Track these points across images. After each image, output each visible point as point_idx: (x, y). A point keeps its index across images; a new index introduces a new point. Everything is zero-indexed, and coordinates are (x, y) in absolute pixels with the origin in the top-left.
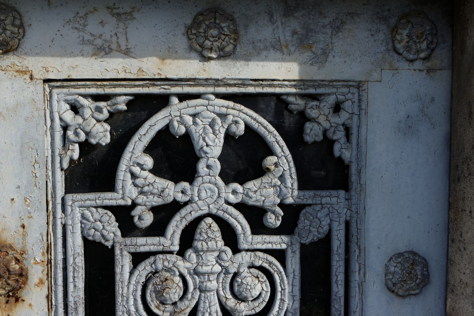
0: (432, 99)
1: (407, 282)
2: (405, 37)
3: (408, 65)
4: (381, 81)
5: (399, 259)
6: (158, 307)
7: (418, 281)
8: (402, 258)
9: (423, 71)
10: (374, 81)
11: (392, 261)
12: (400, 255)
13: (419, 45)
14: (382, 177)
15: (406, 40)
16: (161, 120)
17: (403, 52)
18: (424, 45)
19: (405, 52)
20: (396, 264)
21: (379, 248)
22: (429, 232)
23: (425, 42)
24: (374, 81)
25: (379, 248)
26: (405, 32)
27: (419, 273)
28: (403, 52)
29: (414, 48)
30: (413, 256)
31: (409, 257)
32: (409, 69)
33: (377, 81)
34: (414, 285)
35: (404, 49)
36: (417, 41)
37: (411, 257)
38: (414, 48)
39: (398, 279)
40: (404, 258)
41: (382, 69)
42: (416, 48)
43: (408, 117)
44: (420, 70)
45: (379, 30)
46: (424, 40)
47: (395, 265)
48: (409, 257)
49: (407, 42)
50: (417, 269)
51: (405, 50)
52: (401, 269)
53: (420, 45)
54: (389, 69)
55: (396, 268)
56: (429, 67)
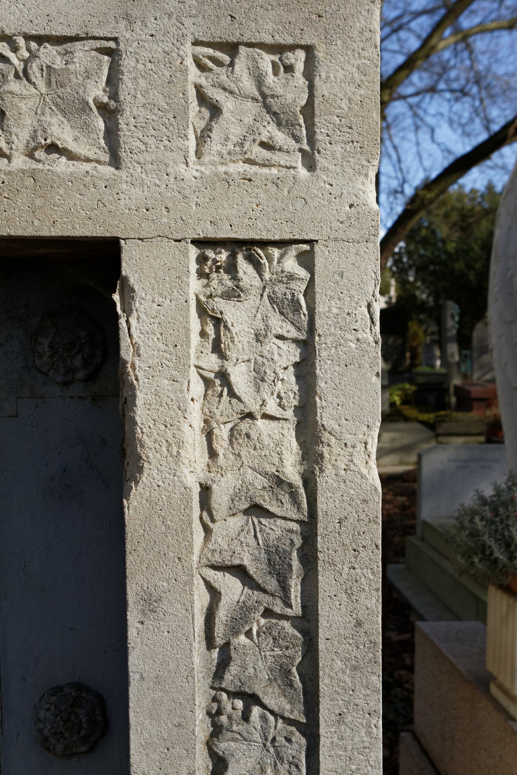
0: (103, 442)
1: (64, 734)
2: (47, 349)
3: (61, 390)
4: (17, 416)
5: (53, 697)
6: (291, 733)
7: (83, 733)
8: (59, 695)
9: (86, 398)
10: (5, 417)
11: (43, 700)
12: (57, 690)
13: (69, 360)
14: (25, 566)
15: (48, 354)
16: (132, 237)
17: (49, 371)
18: (78, 361)
19: (52, 371)
20: (49, 705)
21: (24, 679)
22: (105, 652)
23: (80, 357)
24: (5, 417)
25: (24, 679)
26: (46, 342)
27: (84, 720)
28: (49, 371)
29: (62, 365)
30: (75, 693)
31: (70, 693)
32: (62, 397)
33: (10, 416)
34: (77, 740)
35: (50, 367)
36: (65, 355)
37: (73, 694)
38: (62, 365)
39: (49, 731)
40: (62, 696)
41: (17, 398)
42: (65, 365)
43: (64, 471)
44: (80, 398)
45: (12, 338)
46: (76, 353)
47: (47, 706)
48: (70, 693)
49: (49, 357)
50: (81, 712)
51: (51, 368)
52: (53, 715)
53: (71, 361)
54: (29, 398)
55: (48, 713)
56: (95, 393)
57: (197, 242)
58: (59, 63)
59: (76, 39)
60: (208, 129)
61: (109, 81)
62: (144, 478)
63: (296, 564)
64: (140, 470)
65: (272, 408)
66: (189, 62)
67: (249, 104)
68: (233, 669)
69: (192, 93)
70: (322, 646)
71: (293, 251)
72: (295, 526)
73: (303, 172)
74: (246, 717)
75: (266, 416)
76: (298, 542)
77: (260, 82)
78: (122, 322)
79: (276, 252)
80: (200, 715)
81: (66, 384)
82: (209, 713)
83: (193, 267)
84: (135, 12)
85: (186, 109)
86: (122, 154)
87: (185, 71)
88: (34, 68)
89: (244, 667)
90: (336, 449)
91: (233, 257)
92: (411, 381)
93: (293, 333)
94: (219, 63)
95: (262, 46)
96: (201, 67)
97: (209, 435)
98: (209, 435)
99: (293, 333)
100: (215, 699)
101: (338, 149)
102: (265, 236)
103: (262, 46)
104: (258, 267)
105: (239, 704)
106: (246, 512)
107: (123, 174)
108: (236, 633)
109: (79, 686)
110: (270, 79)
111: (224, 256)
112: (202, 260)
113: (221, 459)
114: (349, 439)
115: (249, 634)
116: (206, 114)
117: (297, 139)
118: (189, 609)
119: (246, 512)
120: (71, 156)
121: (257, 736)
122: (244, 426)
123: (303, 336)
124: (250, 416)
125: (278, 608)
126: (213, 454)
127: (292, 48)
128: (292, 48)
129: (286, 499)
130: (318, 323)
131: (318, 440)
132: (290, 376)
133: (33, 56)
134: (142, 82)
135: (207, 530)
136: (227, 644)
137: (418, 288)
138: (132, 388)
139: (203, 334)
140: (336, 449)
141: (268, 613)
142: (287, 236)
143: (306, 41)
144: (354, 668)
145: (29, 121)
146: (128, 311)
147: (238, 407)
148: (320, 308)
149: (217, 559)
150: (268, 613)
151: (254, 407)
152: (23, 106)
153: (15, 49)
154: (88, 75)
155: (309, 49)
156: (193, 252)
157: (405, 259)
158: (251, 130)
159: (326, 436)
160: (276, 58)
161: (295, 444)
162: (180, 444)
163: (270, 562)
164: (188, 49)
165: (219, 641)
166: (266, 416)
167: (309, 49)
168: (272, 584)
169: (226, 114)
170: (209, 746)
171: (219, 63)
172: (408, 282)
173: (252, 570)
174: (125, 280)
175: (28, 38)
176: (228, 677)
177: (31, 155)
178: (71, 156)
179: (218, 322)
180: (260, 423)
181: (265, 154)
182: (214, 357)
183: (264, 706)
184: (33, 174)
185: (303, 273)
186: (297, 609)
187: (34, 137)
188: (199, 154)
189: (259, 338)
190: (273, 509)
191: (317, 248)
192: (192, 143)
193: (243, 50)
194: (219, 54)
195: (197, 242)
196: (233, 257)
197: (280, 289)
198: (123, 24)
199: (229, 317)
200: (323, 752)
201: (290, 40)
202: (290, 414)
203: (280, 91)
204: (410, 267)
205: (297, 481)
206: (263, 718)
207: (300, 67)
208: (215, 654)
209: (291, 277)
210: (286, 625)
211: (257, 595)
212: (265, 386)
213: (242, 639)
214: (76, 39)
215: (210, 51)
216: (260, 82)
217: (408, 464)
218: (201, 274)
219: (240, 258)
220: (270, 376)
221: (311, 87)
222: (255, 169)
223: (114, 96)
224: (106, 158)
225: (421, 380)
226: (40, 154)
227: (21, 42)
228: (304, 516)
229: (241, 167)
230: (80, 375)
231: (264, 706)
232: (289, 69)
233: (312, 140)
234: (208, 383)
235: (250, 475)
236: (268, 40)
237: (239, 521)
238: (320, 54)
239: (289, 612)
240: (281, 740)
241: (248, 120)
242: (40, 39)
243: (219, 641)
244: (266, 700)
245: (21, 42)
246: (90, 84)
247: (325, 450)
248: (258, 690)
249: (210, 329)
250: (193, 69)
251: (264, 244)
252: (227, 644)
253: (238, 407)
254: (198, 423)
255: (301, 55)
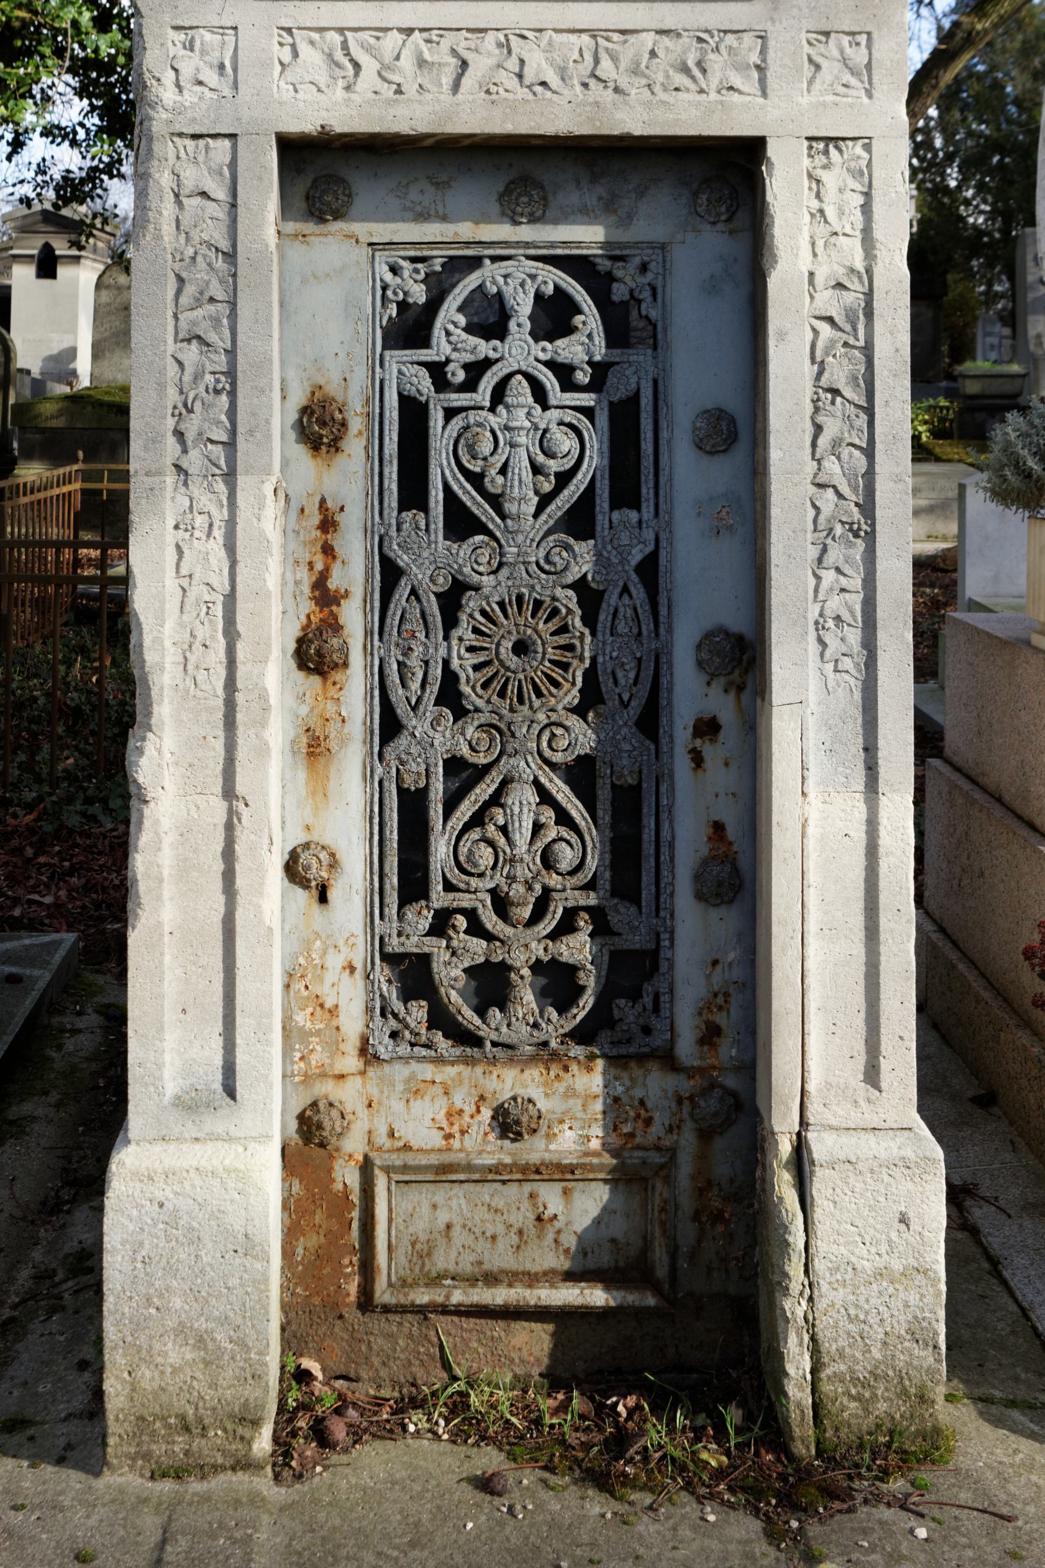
12: (706, 411)
18: (723, 209)
26: (705, 197)
57: (808, 139)
58: (735, 44)
59: (744, 31)
60: (814, 77)
61: (761, 52)
62: (779, 267)
63: (861, 317)
64: (776, 262)
65: (848, 230)
66: (804, 42)
67: (836, 63)
68: (826, 375)
69: (805, 58)
70: (876, 362)
71: (860, 142)
72: (861, 296)
73: (865, 100)
74: (833, 403)
75: (844, 234)
76: (863, 304)
77: (842, 52)
78: (767, 181)
79: (850, 143)
80: (808, 401)
81: (714, 223)
82: (813, 401)
83: (806, 152)
84: (776, 17)
85: (802, 68)
86: (768, 91)
87: (802, 47)
88: (722, 48)
89: (832, 374)
90: (884, 252)
91: (827, 146)
92: (950, 394)
93: (860, 188)
94: (819, 41)
95: (843, 32)
96: (810, 43)
97: (813, 244)
98: (813, 244)
99: (860, 188)
100: (816, 393)
101: (885, 87)
102: (845, 135)
103: (843, 32)
104: (840, 151)
105: (829, 396)
106: (834, 287)
107: (768, 102)
108: (828, 355)
109: (720, 410)
110: (848, 51)
111: (821, 146)
112: (810, 148)
113: (820, 258)
114: (891, 246)
115: (834, 356)
116: (813, 69)
117: (862, 82)
118: (802, 339)
119: (834, 287)
120: (740, 92)
121: (839, 414)
122: (833, 239)
123: (865, 190)
124: (836, 234)
125: (852, 341)
126: (815, 255)
127: (860, 33)
128: (860, 33)
129: (856, 280)
130: (874, 182)
131: (874, 248)
132: (858, 212)
133: (721, 40)
134: (779, 54)
135: (812, 297)
136: (823, 362)
137: (967, 202)
138: (772, 217)
139: (810, 189)
140: (884, 252)
141: (846, 344)
142: (857, 135)
143: (867, 29)
144: (895, 375)
145: (718, 75)
146: (771, 176)
147: (829, 229)
148: (875, 174)
149: (817, 313)
150: (846, 344)
151: (838, 229)
152: (716, 67)
153: (712, 37)
154: (750, 49)
155: (869, 34)
156: (806, 143)
157: (938, 143)
158: (837, 78)
159: (878, 245)
160: (850, 38)
161: (860, 250)
162: (798, 248)
163: (847, 316)
164: (804, 36)
165: (818, 359)
166: (844, 234)
167: (869, 34)
168: (848, 328)
169: (824, 70)
170: (813, 419)
171: (819, 41)
172: (947, 190)
173: (837, 319)
174: (769, 159)
175: (719, 31)
176: (823, 379)
177: (719, 92)
178: (740, 92)
179: (818, 181)
180: (841, 238)
181: (844, 90)
182: (816, 201)
183: (843, 397)
184: (722, 103)
185: (866, 155)
186: (862, 343)
187: (721, 82)
188: (809, 91)
189: (841, 191)
190: (849, 285)
191: (874, 141)
192: (805, 85)
193: (833, 35)
194: (820, 37)
195: (808, 139)
196: (827, 146)
197: (853, 164)
198: (769, 23)
199: (824, 179)
200: (877, 422)
201: (858, 29)
202: (858, 233)
203: (853, 56)
204: (950, 158)
205: (863, 271)
206: (843, 404)
207: (864, 43)
208: (816, 367)
209: (859, 157)
210: (856, 352)
211: (840, 334)
212: (844, 218)
213: (831, 359)
214: (744, 31)
215: (815, 36)
216: (842, 52)
217: (945, 539)
218: (810, 156)
219: (831, 147)
220: (847, 212)
221: (870, 54)
222: (838, 99)
223: (764, 60)
224: (759, 93)
225: (972, 388)
226: (724, 92)
227: (716, 33)
228: (866, 290)
229: (830, 98)
230: (723, 218)
231: (843, 397)
232: (858, 44)
233: (870, 83)
234: (812, 215)
235: (836, 267)
236: (847, 29)
237: (830, 292)
238: (875, 36)
239: (858, 344)
240: (853, 417)
241: (836, 72)
242: (725, 32)
243: (818, 359)
244: (844, 393)
245: (716, 33)
246: (751, 54)
247: (878, 253)
248: (840, 386)
249: (814, 186)
250: (806, 46)
251: (844, 139)
252: (823, 362)
253: (829, 229)
254: (808, 238)
255: (865, 36)
